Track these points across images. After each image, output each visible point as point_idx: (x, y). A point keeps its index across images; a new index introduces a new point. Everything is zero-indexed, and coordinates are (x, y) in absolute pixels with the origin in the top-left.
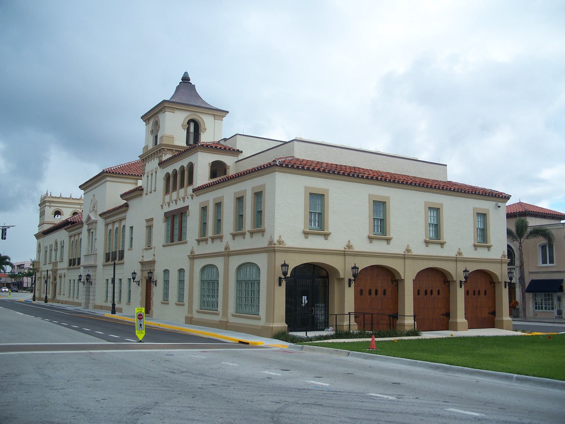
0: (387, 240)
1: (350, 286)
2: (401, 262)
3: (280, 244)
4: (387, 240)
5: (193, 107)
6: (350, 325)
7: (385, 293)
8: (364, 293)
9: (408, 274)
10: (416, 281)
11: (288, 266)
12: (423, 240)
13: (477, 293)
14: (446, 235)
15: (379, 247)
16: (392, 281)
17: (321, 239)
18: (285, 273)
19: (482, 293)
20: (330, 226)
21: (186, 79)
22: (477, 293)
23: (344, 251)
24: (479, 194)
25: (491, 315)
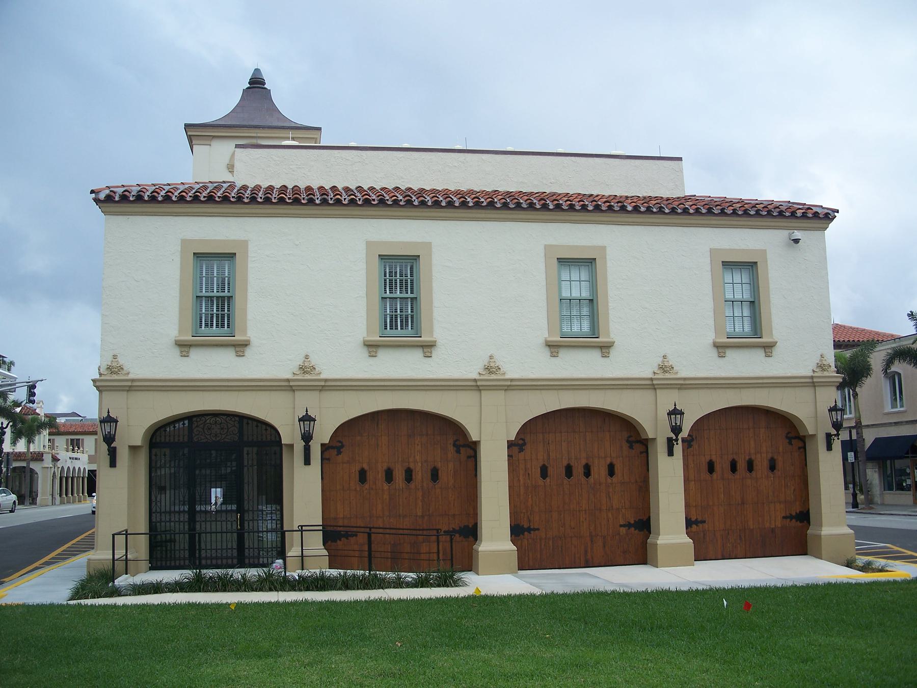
0: (601, 347)
1: (671, 453)
2: (470, 397)
3: (824, 370)
4: (601, 347)
5: (246, 130)
6: (302, 556)
7: (435, 475)
8: (370, 476)
9: (494, 430)
10: (516, 447)
11: (116, 421)
12: (541, 341)
13: (742, 465)
14: (617, 325)
15: (214, 365)
16: (458, 448)
18: (676, 430)
19: (761, 464)
20: (250, 324)
21: (257, 82)
22: (742, 465)
23: (812, 377)
25: (794, 523)
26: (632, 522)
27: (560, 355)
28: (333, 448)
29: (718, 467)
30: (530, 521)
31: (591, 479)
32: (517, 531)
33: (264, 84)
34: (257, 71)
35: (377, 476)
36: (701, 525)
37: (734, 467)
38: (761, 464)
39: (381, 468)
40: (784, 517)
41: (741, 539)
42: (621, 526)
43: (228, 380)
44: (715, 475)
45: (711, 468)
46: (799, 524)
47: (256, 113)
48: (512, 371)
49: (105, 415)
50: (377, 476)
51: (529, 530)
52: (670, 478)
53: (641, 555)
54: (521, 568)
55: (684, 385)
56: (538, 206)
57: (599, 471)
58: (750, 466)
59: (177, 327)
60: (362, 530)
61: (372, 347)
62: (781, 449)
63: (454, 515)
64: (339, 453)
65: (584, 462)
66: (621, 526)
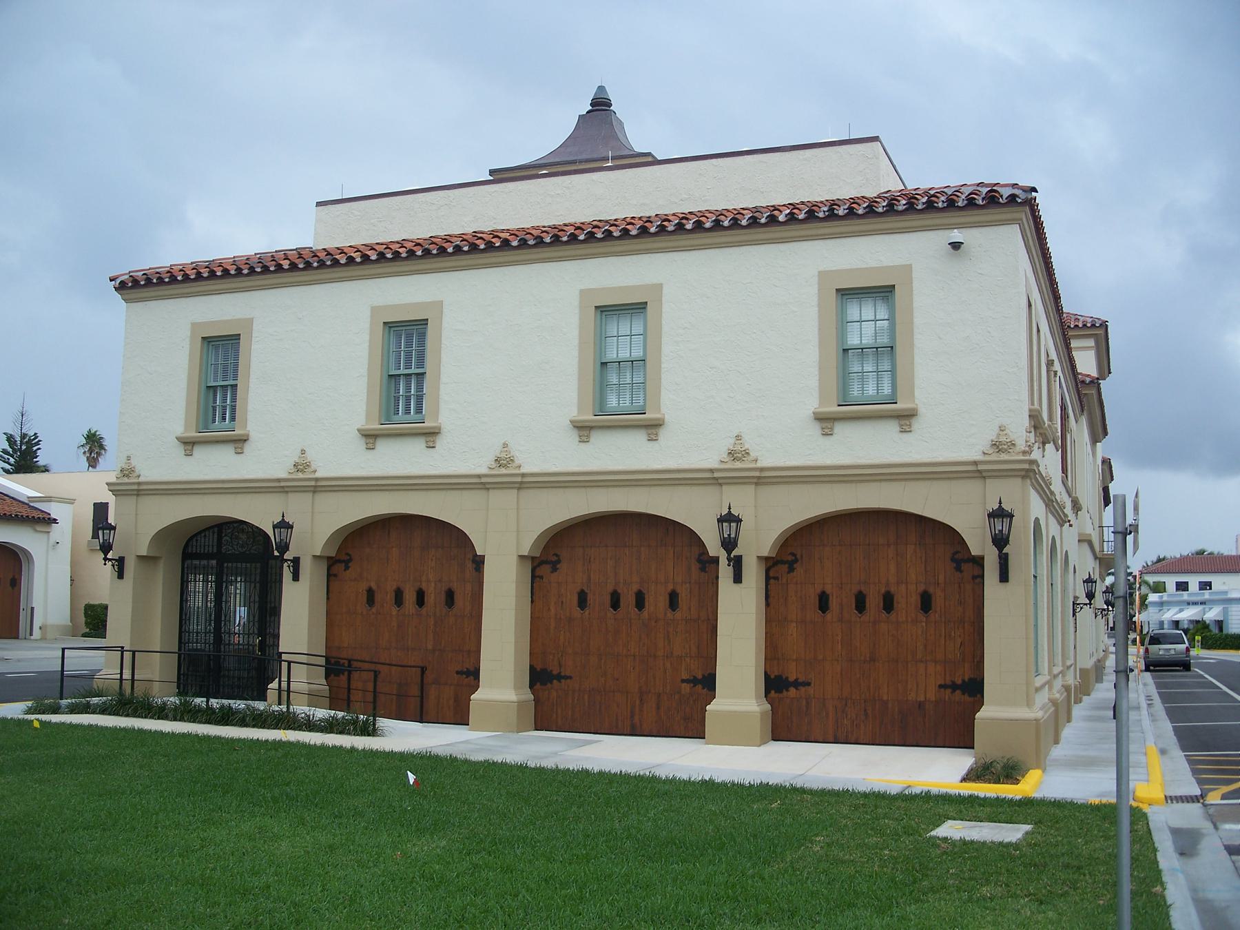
8: (378, 597)
9: (503, 543)
11: (1011, 516)
13: (874, 602)
14: (674, 396)
17: (637, 439)
19: (907, 601)
21: (601, 104)
22: (874, 602)
26: (700, 677)
27: (592, 439)
28: (339, 561)
29: (834, 603)
30: (560, 666)
31: (645, 613)
32: (774, 685)
33: (610, 105)
34: (601, 89)
35: (385, 597)
36: (803, 689)
37: (860, 603)
38: (907, 601)
39: (391, 587)
40: (941, 686)
41: (866, 715)
42: (683, 681)
43: (223, 482)
44: (829, 616)
45: (823, 602)
46: (967, 698)
48: (531, 463)
49: (725, 512)
50: (385, 597)
51: (559, 677)
52: (739, 615)
53: (693, 729)
54: (777, 737)
55: (763, 479)
56: (435, 252)
57: (657, 602)
58: (888, 603)
59: (182, 422)
60: (366, 666)
61: (371, 437)
62: (941, 578)
63: (469, 651)
64: (347, 568)
65: (635, 588)
66: (683, 681)
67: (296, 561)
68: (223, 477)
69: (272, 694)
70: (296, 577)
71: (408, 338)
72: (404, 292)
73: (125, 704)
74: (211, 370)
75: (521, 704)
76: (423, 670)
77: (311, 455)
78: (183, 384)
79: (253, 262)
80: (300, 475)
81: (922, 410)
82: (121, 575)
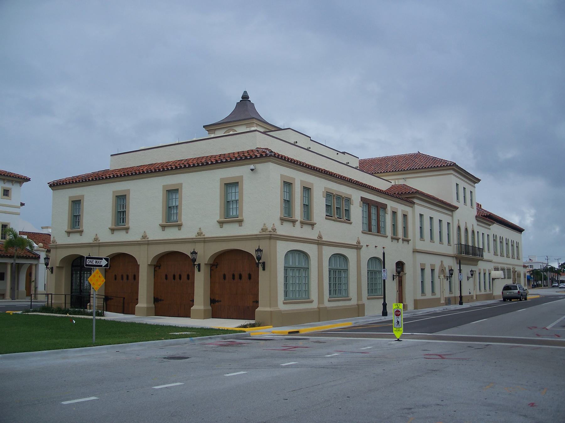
9: (144, 259)
11: (262, 251)
13: (237, 277)
20: (84, 224)
21: (245, 97)
22: (237, 277)
24: (194, 166)
47: (244, 111)
51: (161, 300)
53: (187, 315)
61: (113, 230)
67: (199, 265)
68: (246, 234)
69: (88, 307)
70: (199, 270)
71: (121, 200)
72: (171, 180)
73: (59, 311)
74: (119, 206)
75: (205, 311)
76: (124, 298)
77: (203, 230)
78: (67, 215)
79: (231, 155)
80: (264, 233)
81: (245, 219)
82: (52, 273)
